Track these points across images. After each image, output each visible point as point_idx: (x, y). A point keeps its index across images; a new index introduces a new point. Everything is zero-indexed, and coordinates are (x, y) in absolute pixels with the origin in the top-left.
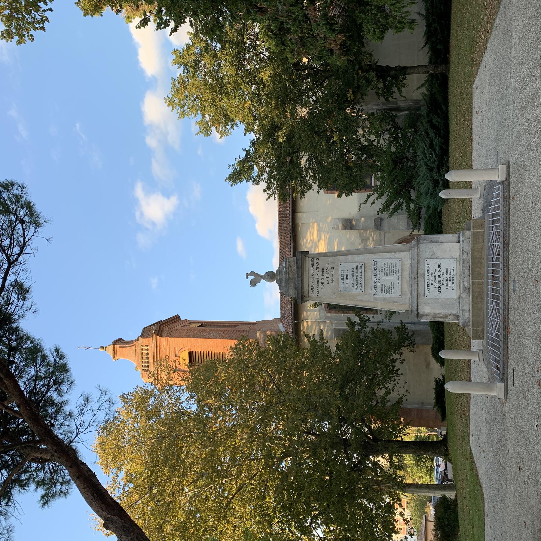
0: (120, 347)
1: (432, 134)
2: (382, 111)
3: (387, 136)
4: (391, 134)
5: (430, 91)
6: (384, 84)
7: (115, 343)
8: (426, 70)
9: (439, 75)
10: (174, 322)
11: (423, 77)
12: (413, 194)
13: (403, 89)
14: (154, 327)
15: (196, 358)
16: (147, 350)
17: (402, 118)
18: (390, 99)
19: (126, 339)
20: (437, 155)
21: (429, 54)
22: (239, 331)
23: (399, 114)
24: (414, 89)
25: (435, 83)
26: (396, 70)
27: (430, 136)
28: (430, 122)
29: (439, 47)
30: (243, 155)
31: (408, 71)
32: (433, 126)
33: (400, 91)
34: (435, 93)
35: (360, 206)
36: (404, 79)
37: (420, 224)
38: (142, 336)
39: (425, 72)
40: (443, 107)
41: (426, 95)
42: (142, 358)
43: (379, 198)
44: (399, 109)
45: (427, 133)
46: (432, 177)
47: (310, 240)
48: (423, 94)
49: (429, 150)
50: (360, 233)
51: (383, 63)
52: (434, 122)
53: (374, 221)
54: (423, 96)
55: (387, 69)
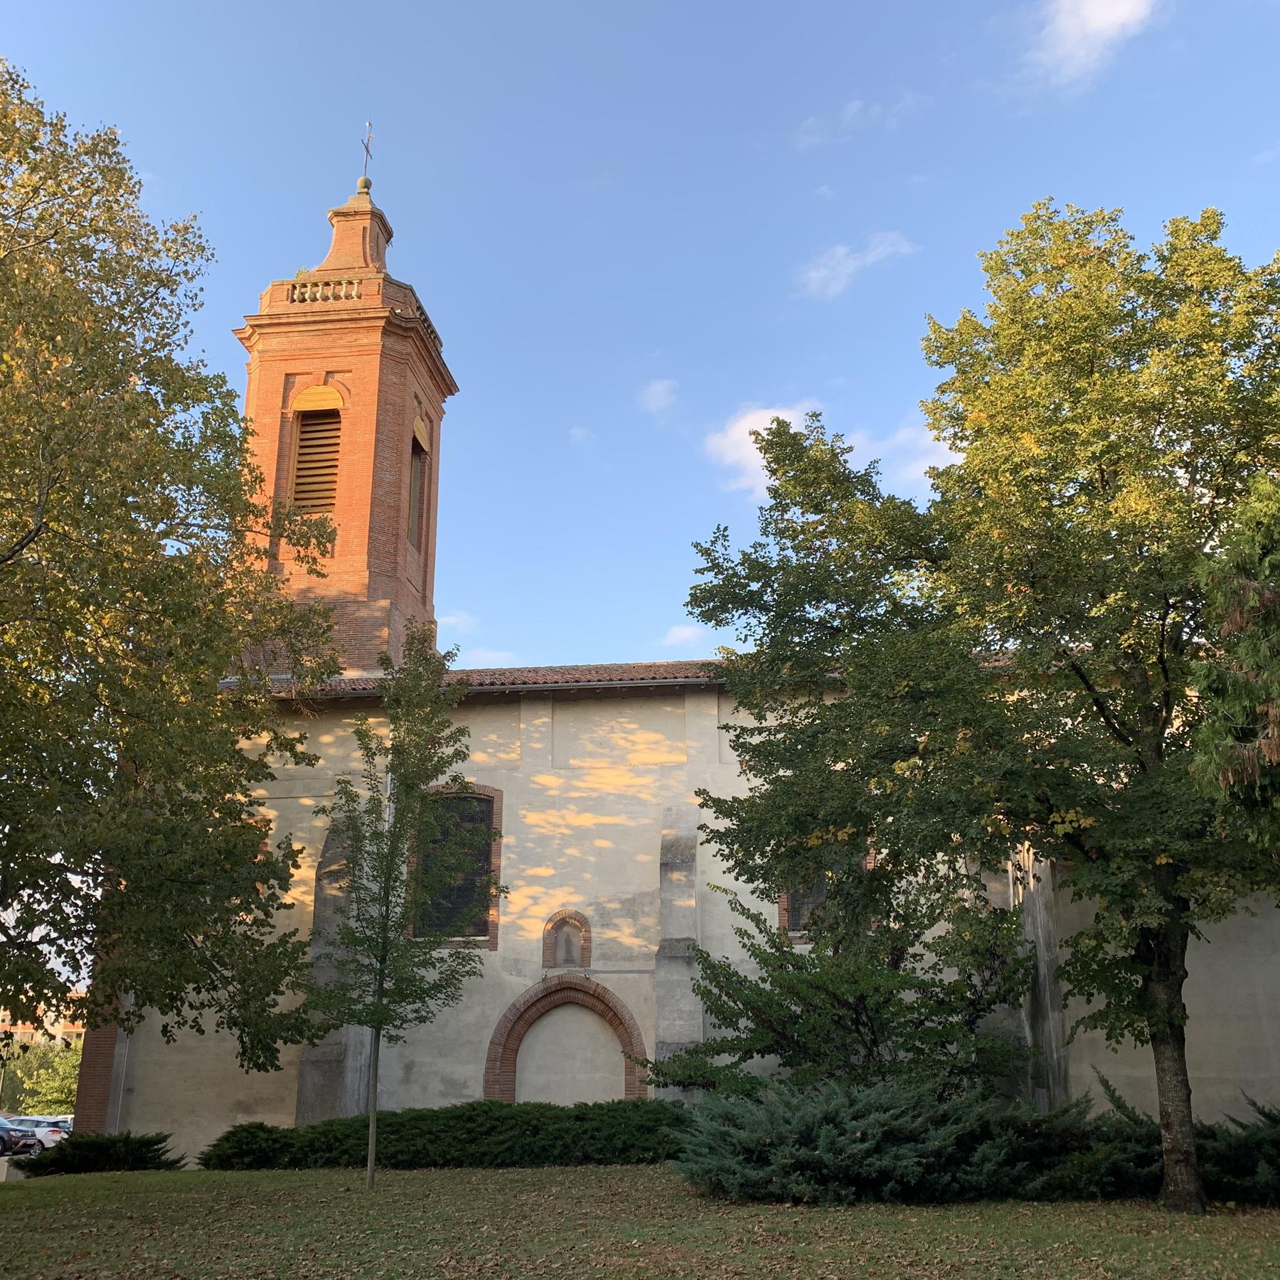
0: (364, 228)
1: (939, 1139)
2: (1029, 958)
3: (950, 975)
4: (952, 989)
5: (1097, 1133)
6: (1117, 963)
7: (377, 216)
8: (1174, 1119)
9: (1155, 1167)
10: (432, 377)
11: (1147, 1103)
12: (762, 1065)
13: (1101, 1033)
14: (410, 313)
15: (321, 433)
16: (348, 297)
17: (1009, 1024)
18: (1066, 986)
19: (390, 252)
20: (859, 1160)
21: (1233, 1128)
22: (396, 549)
23: (1023, 1014)
24: (1106, 1073)
25: (1125, 1150)
26: (1171, 1007)
27: (932, 1132)
28: (984, 1133)
29: (1264, 1172)
30: (856, 464)
31: (1168, 1052)
32: (967, 1143)
33: (1093, 1021)
34: (1089, 1148)
35: (725, 891)
36: (1139, 1037)
37: (666, 1085)
38: (388, 280)
39: (1164, 1114)
40: (1040, 1181)
41: (1082, 1114)
42: (327, 284)
43: (755, 951)
44: (1037, 1016)
45: (942, 1121)
46: (782, 1140)
47: (634, 743)
48: (1087, 1101)
49: (878, 1131)
50: (651, 895)
51: (1195, 957)
52: (984, 1148)
53: (685, 935)
54: (1077, 1105)
55: (1174, 975)
